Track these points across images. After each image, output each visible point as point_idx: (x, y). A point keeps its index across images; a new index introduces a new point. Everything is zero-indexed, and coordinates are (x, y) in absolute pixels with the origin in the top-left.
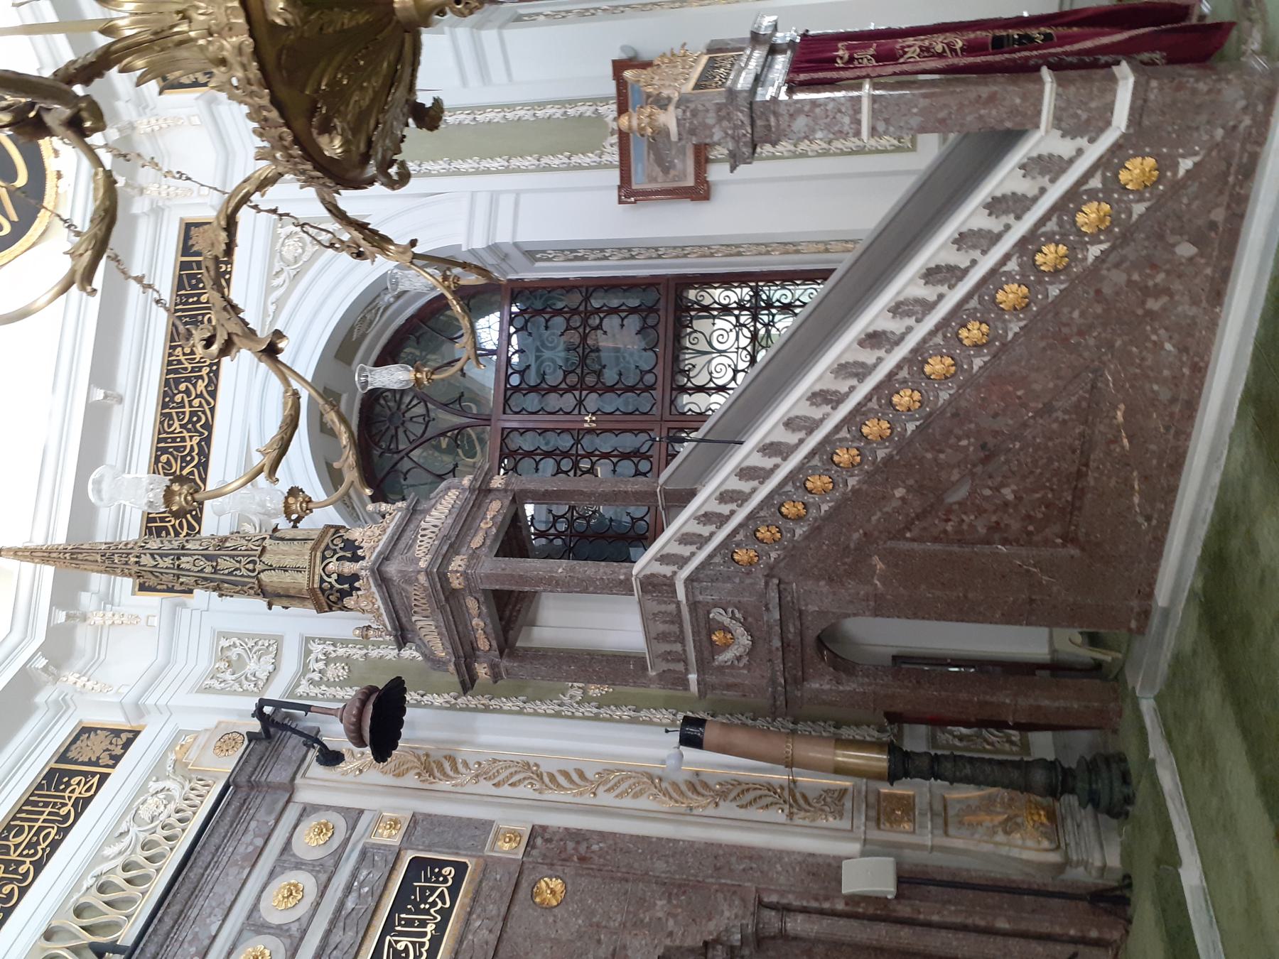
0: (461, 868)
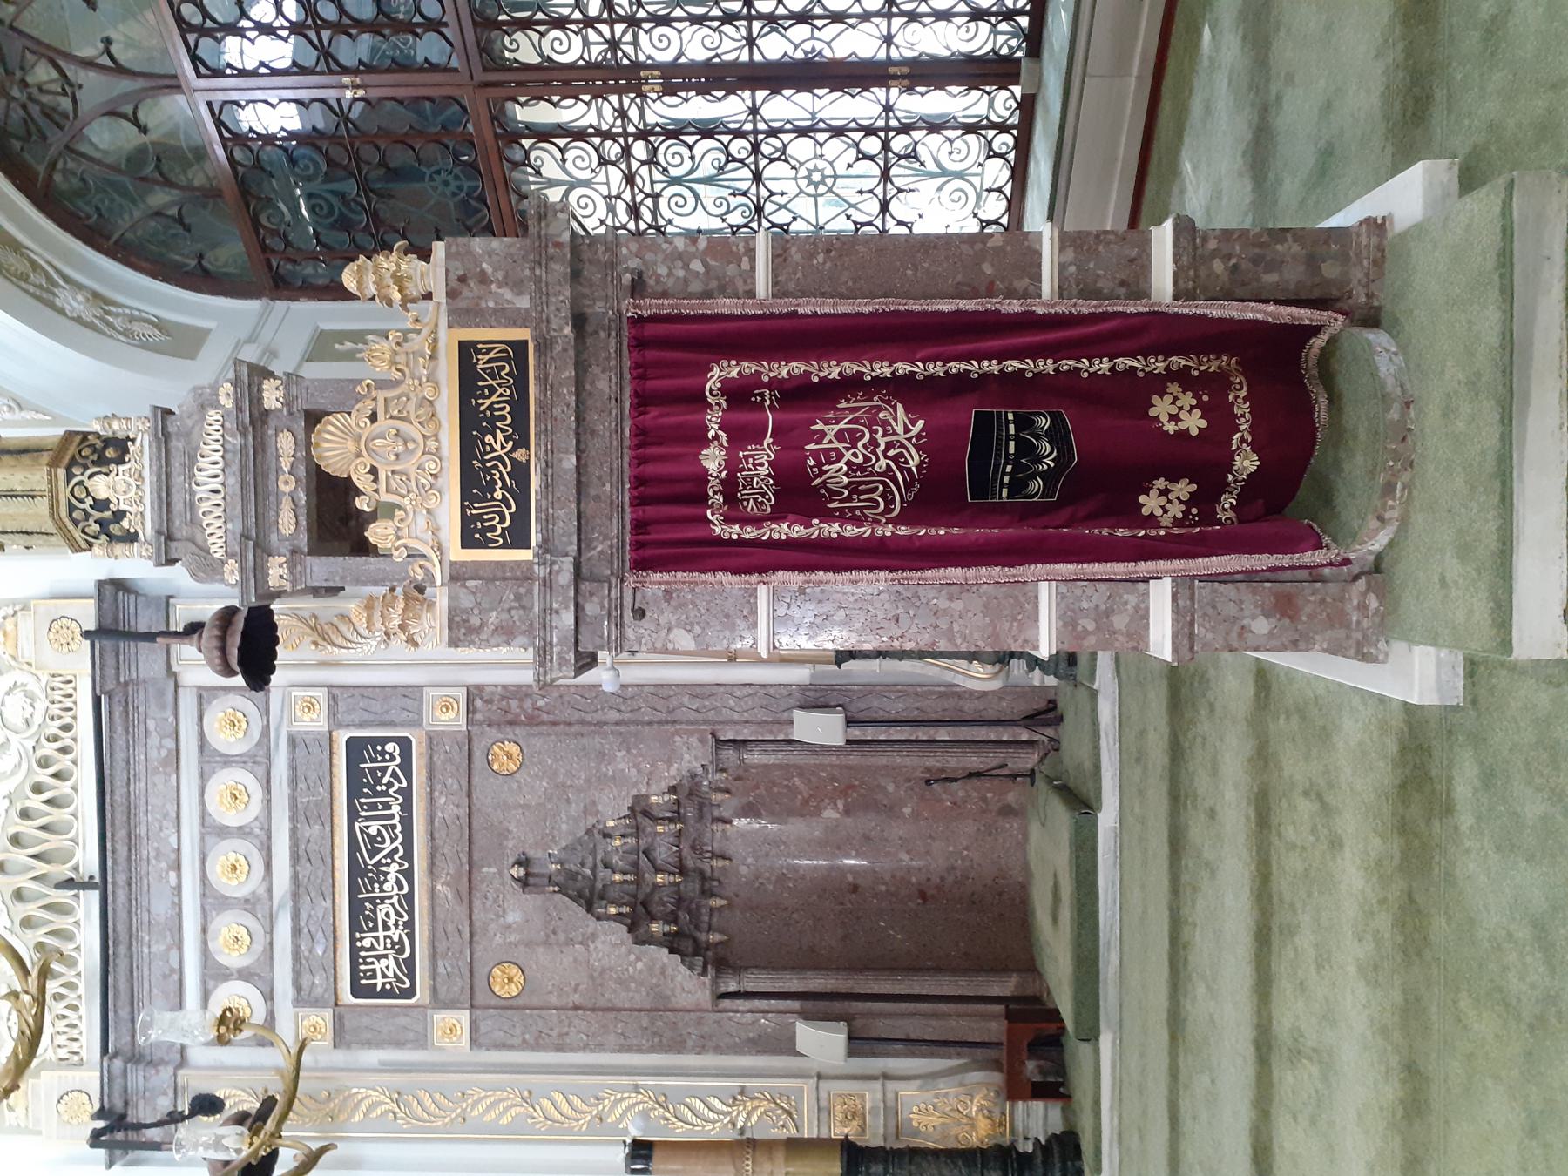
0: (404, 744)
